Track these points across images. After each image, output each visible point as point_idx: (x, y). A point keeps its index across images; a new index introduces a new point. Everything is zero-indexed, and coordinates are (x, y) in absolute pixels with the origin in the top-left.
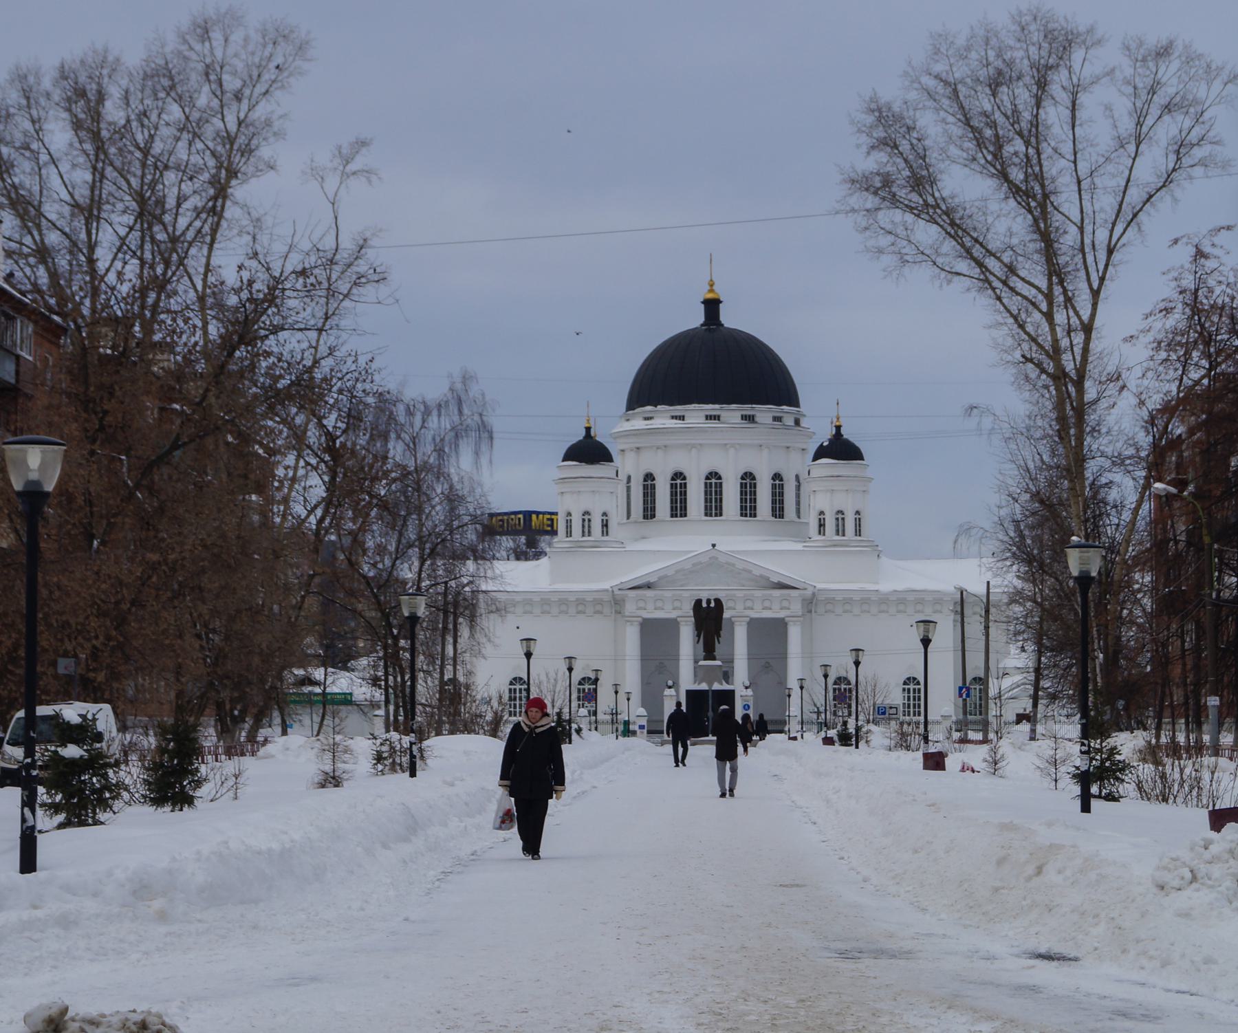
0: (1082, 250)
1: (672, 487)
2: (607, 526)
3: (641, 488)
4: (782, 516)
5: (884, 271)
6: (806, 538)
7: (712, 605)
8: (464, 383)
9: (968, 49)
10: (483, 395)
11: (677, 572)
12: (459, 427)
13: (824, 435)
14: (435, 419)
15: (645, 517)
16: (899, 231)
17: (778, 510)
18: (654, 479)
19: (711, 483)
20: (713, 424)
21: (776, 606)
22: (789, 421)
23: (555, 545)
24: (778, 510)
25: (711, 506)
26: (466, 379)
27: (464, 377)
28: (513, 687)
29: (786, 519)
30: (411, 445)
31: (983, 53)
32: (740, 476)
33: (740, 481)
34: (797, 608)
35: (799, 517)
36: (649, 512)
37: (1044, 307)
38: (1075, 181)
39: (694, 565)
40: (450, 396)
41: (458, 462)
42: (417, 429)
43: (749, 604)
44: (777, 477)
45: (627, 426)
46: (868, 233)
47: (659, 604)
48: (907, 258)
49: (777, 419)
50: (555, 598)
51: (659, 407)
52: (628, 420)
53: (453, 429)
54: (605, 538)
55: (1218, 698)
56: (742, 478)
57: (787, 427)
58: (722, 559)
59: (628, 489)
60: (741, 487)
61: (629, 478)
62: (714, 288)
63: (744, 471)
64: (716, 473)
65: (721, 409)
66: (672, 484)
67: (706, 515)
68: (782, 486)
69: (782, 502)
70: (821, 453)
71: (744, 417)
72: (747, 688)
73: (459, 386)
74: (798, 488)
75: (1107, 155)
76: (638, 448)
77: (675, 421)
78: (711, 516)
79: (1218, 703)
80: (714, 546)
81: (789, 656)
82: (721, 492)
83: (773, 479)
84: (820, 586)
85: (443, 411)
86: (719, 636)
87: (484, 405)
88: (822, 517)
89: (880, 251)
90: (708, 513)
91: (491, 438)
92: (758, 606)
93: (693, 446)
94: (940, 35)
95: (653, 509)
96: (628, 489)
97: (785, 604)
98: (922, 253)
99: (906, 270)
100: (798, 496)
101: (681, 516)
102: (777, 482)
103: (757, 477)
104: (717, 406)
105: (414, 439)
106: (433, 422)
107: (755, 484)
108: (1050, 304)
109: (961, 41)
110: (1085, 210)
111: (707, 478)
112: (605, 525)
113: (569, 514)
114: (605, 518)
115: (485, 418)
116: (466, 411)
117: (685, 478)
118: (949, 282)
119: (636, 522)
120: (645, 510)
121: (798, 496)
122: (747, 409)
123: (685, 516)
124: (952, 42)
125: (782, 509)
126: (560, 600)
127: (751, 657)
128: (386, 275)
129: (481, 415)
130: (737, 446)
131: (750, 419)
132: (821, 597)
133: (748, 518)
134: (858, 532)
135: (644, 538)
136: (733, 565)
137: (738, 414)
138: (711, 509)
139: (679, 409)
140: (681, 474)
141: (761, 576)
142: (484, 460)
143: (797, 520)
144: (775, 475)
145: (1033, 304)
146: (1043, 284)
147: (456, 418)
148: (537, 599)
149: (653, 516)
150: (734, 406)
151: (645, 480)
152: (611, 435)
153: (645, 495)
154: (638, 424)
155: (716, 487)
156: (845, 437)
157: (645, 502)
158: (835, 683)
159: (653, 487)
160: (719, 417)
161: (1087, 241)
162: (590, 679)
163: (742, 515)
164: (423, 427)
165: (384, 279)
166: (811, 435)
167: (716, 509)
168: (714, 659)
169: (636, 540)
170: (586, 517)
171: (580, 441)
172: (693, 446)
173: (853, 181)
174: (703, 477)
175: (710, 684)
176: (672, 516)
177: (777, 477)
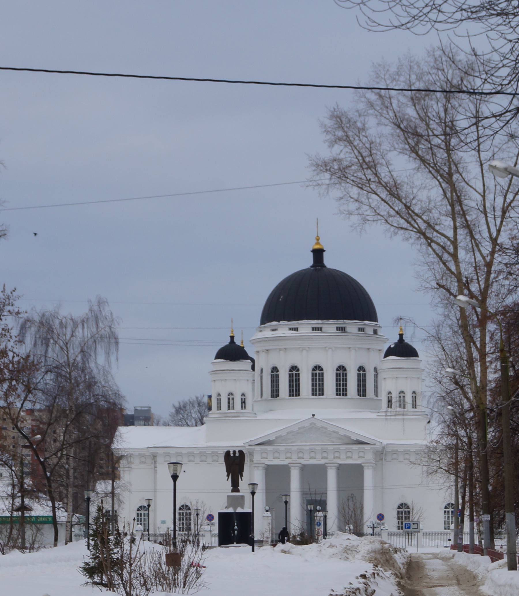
0: (485, 212)
1: (290, 376)
2: (245, 402)
3: (270, 377)
4: (364, 395)
5: (351, 226)
6: (376, 409)
7: (237, 454)
8: (99, 306)
9: (398, 74)
10: (111, 313)
11: (288, 433)
12: (97, 336)
13: (392, 340)
14: (80, 329)
15: (272, 396)
16: (363, 200)
17: (362, 391)
18: (278, 371)
19: (316, 374)
20: (317, 333)
21: (355, 456)
22: (370, 331)
23: (210, 416)
24: (362, 391)
25: (316, 389)
26: (101, 303)
27: (99, 302)
28: (139, 512)
29: (348, 396)
30: (65, 348)
31: (408, 77)
32: (335, 369)
33: (335, 371)
34: (369, 457)
35: (377, 396)
36: (275, 393)
37: (451, 249)
38: (479, 164)
39: (299, 428)
40: (90, 315)
41: (96, 359)
42: (68, 338)
43: (337, 455)
44: (361, 369)
45: (260, 335)
46: (342, 201)
47: (349, 454)
48: (368, 218)
49: (361, 330)
50: (209, 451)
51: (281, 322)
52: (261, 331)
53: (92, 337)
54: (243, 411)
55: (489, 516)
56: (337, 370)
57: (368, 335)
58: (319, 424)
59: (261, 377)
61: (262, 370)
62: (320, 241)
63: (338, 365)
64: (320, 367)
65: (322, 324)
66: (290, 374)
67: (313, 395)
68: (364, 375)
69: (364, 386)
70: (389, 352)
71: (338, 329)
72: (267, 511)
73: (96, 308)
74: (376, 376)
75: (499, 146)
76: (267, 350)
77: (291, 331)
78: (316, 395)
79: (489, 519)
80: (313, 415)
81: (365, 488)
82: (323, 379)
83: (359, 370)
84: (385, 442)
85: (85, 325)
86: (242, 476)
87: (112, 321)
88: (390, 395)
89: (350, 213)
91: (117, 343)
92: (343, 456)
93: (304, 349)
94: (379, 65)
95: (278, 391)
96: (261, 377)
97: (361, 454)
98: (379, 214)
99: (367, 226)
100: (376, 381)
101: (296, 396)
102: (361, 372)
103: (324, 368)
104: (320, 321)
105: (66, 344)
106: (79, 332)
107: (346, 374)
108: (456, 248)
109: (393, 69)
110: (486, 184)
111: (313, 370)
112: (243, 402)
113: (219, 395)
114: (243, 397)
115: (113, 330)
116: (101, 325)
117: (298, 370)
118: (396, 234)
119: (266, 400)
120: (272, 391)
121: (376, 381)
122: (340, 323)
123: (299, 395)
124: (388, 70)
125: (365, 390)
126: (213, 453)
127: (339, 489)
128: (6, 232)
129: (110, 327)
130: (334, 349)
131: (342, 330)
132: (389, 450)
133: (341, 397)
134: (415, 406)
135: (271, 411)
136: (326, 428)
137: (335, 326)
138: (316, 391)
139: (294, 324)
140: (296, 367)
141: (345, 436)
142: (113, 358)
143: (375, 398)
145: (444, 248)
146: (450, 234)
147: (94, 330)
148: (196, 452)
149: (278, 396)
150: (331, 321)
151: (272, 372)
152: (250, 341)
153: (272, 381)
154: (267, 333)
155: (319, 376)
156: (406, 341)
157: (272, 386)
158: (180, 509)
159: (277, 376)
160: (321, 328)
161: (488, 205)
162: (145, 507)
163: (337, 395)
164: (72, 336)
165: (5, 234)
166: (385, 341)
167: (319, 391)
168: (238, 491)
169: (266, 412)
170: (231, 397)
171: (227, 346)
172: (304, 349)
173: (317, 165)
174: (311, 369)
175: (235, 508)
176: (290, 396)
177: (361, 369)
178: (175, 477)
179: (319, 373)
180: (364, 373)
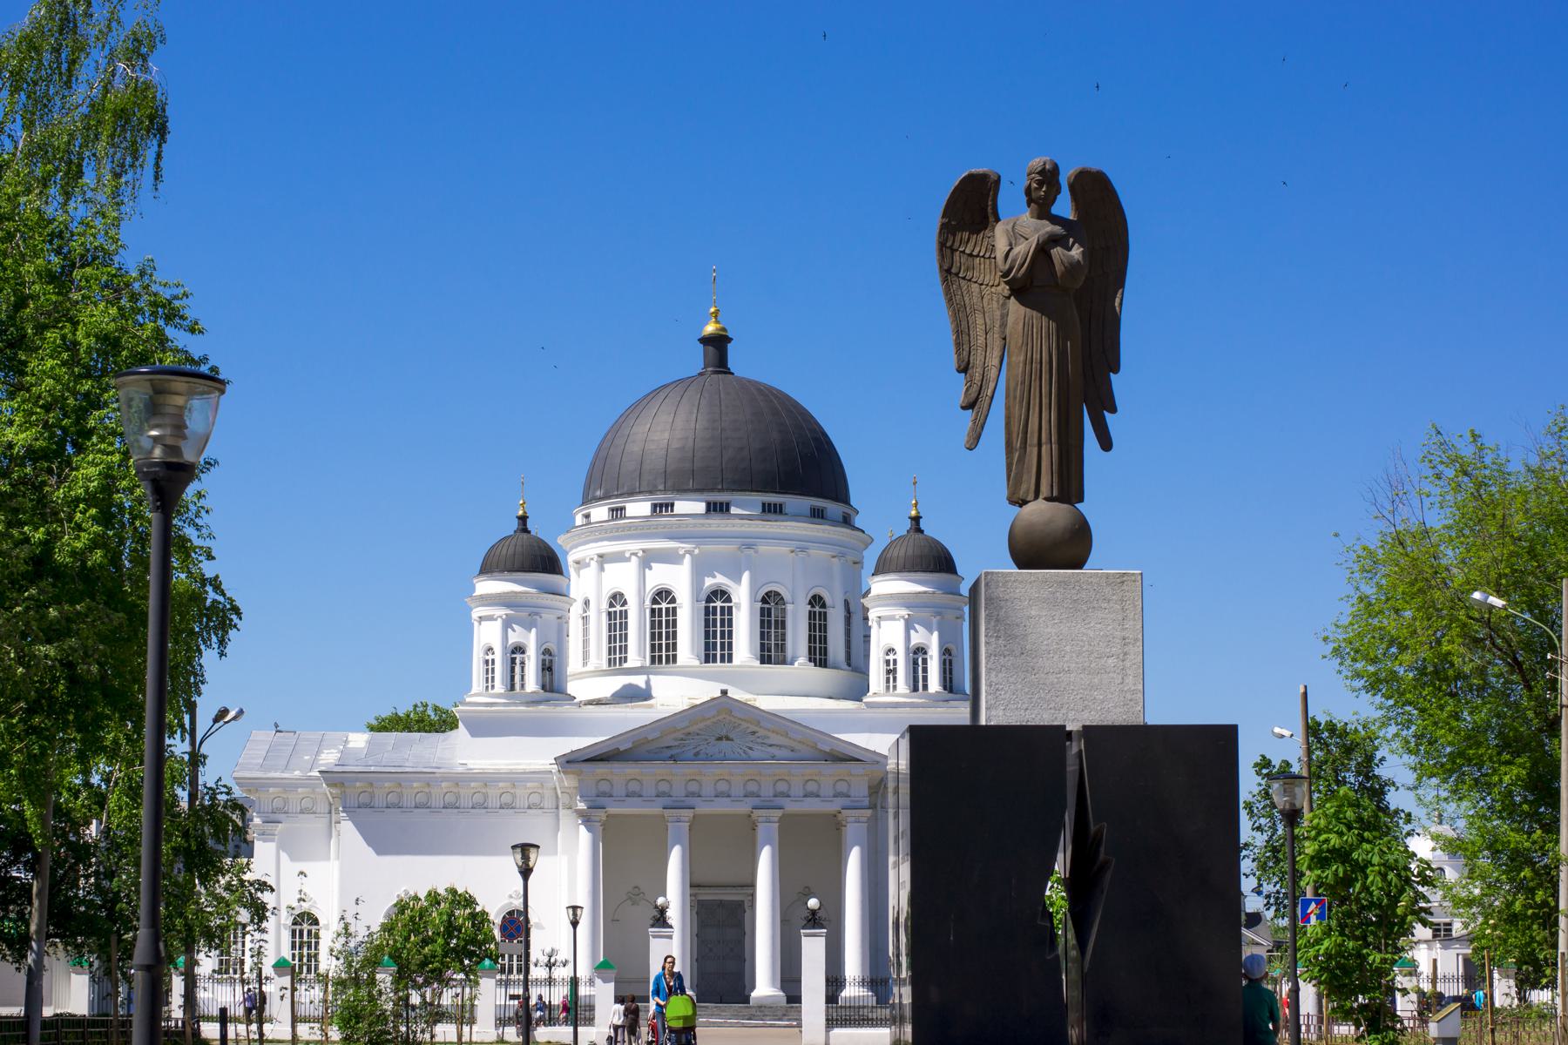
2: (550, 669)
19: (715, 608)
33: (759, 605)
60: (762, 615)
65: (588, 508)
68: (824, 616)
90: (765, 659)
102: (817, 609)
117: (673, 600)
140: (668, 592)
144: (814, 597)
151: (611, 605)
155: (722, 613)
170: (518, 657)
178: (526, 872)
179: (722, 608)
180: (623, 608)
